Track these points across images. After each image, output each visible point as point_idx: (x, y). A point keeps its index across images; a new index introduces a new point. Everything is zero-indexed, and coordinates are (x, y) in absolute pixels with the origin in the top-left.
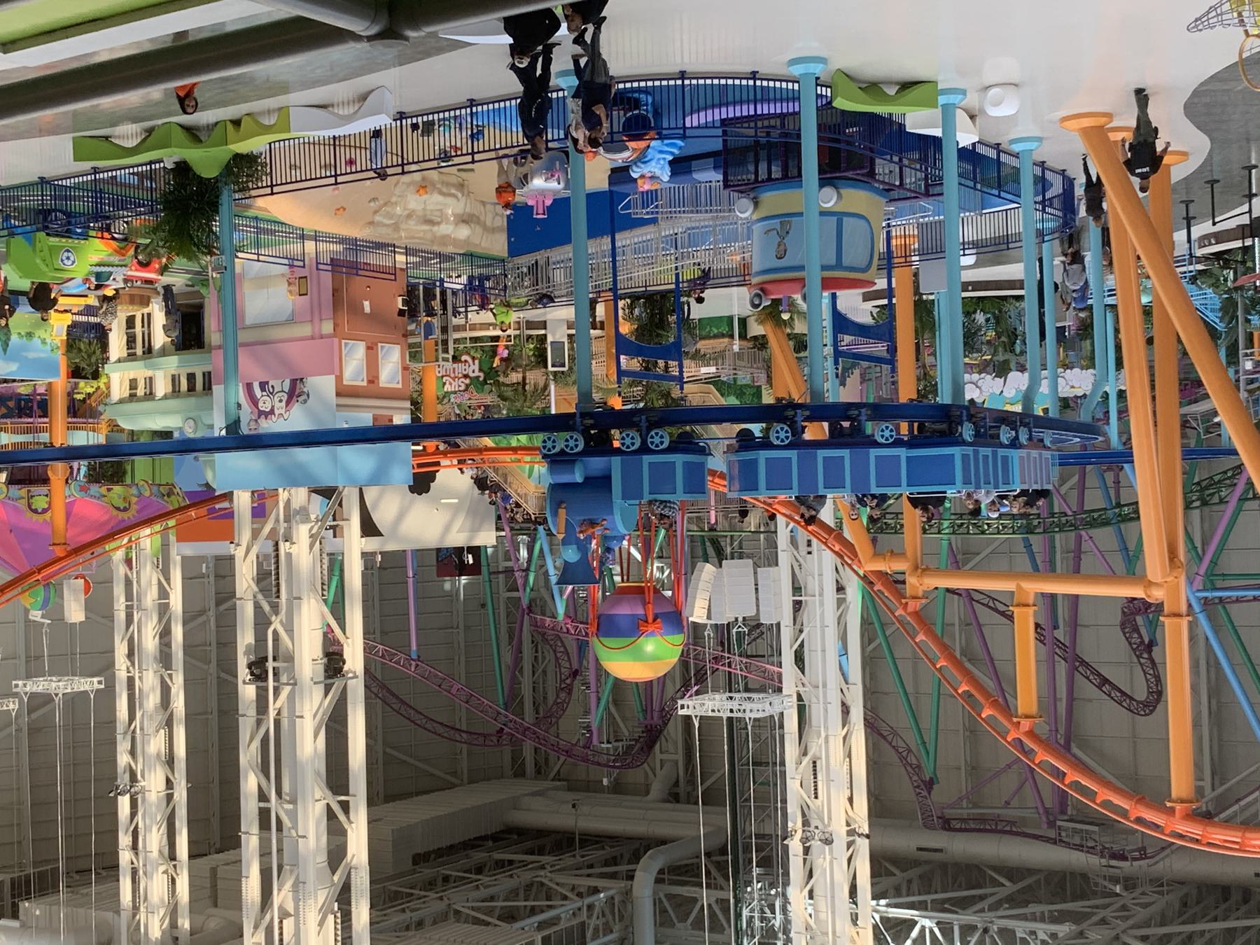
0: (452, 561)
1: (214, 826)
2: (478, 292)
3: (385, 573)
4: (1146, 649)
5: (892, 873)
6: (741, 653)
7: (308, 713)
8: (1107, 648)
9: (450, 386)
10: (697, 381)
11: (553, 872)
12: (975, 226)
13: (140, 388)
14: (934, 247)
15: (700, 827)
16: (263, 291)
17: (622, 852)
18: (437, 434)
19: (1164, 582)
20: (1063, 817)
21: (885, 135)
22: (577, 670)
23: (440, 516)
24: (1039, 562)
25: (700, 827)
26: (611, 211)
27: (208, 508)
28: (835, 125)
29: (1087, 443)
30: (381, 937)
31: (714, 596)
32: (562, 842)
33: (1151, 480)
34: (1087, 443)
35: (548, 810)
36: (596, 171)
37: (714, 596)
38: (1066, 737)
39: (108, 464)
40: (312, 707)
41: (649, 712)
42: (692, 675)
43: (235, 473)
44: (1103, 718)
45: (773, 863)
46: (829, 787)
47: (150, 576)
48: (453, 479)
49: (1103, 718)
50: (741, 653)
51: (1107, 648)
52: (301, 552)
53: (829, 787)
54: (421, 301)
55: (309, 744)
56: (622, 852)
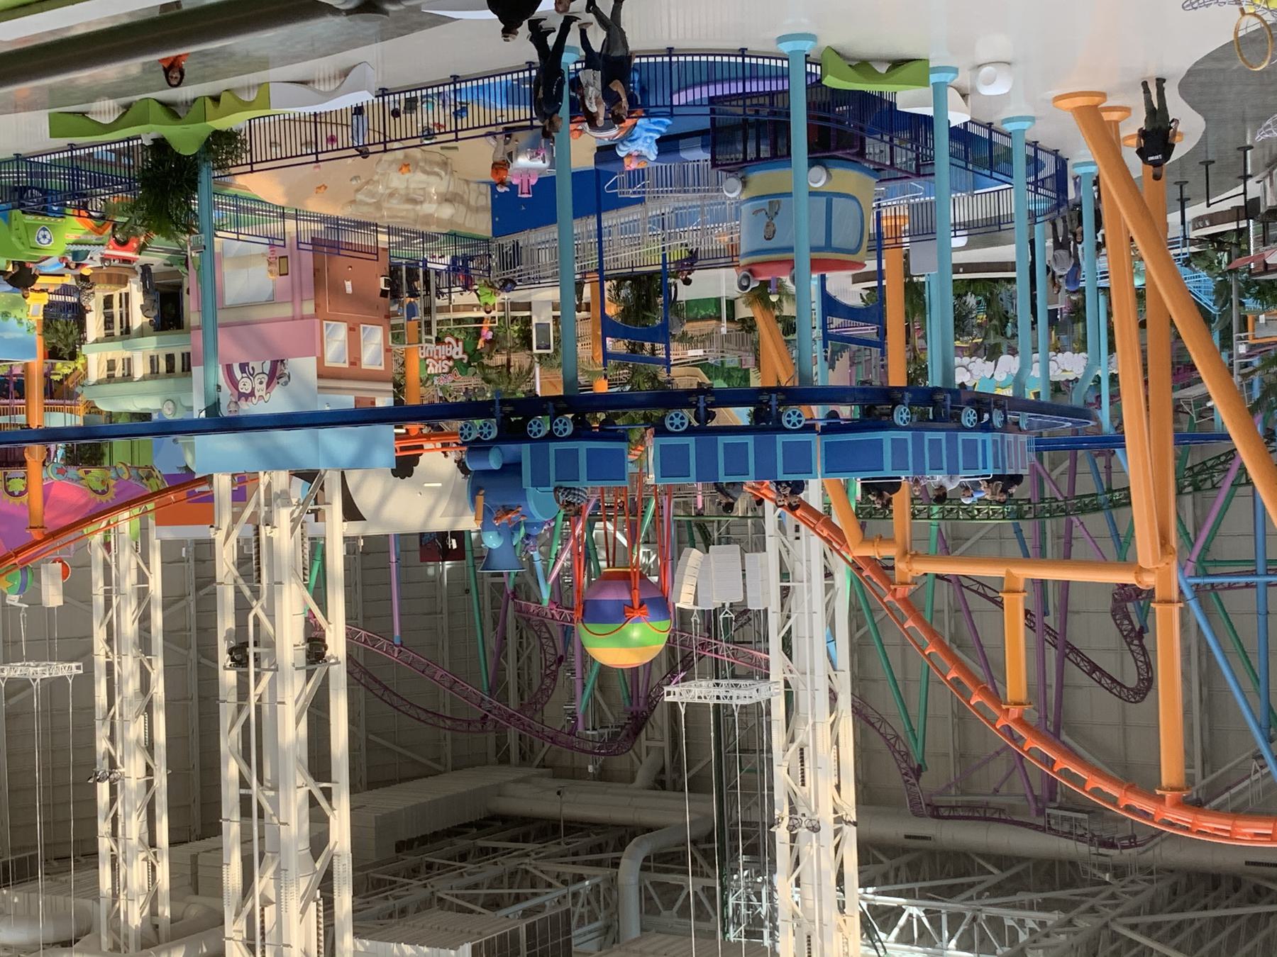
0: (435, 545)
1: (194, 813)
2: (462, 272)
3: (367, 557)
4: (1137, 637)
5: (879, 861)
6: (728, 639)
9: (434, 369)
11: (537, 859)
12: (966, 207)
13: (117, 369)
14: (924, 228)
15: (686, 814)
16: (243, 271)
17: (608, 839)
19: (1155, 568)
21: (877, 115)
22: (563, 656)
25: (686, 814)
26: (597, 191)
27: (188, 491)
28: (824, 103)
31: (701, 581)
32: (546, 830)
33: (1143, 465)
35: (532, 796)
37: (701, 581)
38: (1055, 724)
39: (86, 446)
40: (293, 693)
41: (635, 699)
42: (678, 661)
43: (215, 456)
45: (759, 851)
46: (816, 774)
47: (129, 559)
50: (728, 639)
51: (1097, 635)
52: (282, 536)
53: (816, 774)
54: (404, 281)
55: (291, 730)
56: (608, 839)
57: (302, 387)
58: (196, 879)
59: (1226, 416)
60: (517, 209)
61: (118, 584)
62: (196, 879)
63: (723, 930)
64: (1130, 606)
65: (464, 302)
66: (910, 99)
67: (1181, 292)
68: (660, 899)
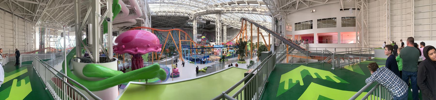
0: (212, 42)
1: (222, 30)
2: (210, 54)
3: (215, 41)
4: (181, 38)
5: (192, 28)
6: (199, 37)
7: (218, 35)
8: (183, 38)
9: (212, 50)
10: (201, 50)
11: (208, 28)
12: (188, 56)
13: (225, 49)
14: (190, 56)
15: (201, 30)
16: (220, 54)
17: (204, 28)
18: (213, 48)
19: (180, 41)
20: (185, 30)
21: (192, 61)
22: (206, 37)
23: (212, 44)
24: (211, 15)
25: (201, 30)
26: (205, 57)
27: (223, 44)
28: (194, 61)
29: (184, 46)
30: (139, 66)
31: (200, 40)
32: (207, 29)
33: (181, 45)
34: (184, 46)
35: (208, 30)
36: (205, 59)
37: (200, 40)
38: (185, 34)
39: (227, 46)
40: (218, 35)
41: (203, 35)
42: (201, 36)
43: (222, 46)
44: (183, 35)
45: (197, 28)
46: (195, 31)
47: (225, 41)
48: (212, 45)
49: (183, 35)
50: (199, 37)
51: (183, 38)
52: (219, 42)
53: (195, 31)
54: (213, 53)
55: (218, 34)
56: (204, 28)
57: (217, 49)
58: (222, 28)
59: (177, 47)
60: (208, 57)
61: (180, 7)
62: (222, 28)
63: (134, 65)
64: (181, 39)
65: (210, 52)
66: (190, 61)
67: (179, 52)
68: (202, 26)
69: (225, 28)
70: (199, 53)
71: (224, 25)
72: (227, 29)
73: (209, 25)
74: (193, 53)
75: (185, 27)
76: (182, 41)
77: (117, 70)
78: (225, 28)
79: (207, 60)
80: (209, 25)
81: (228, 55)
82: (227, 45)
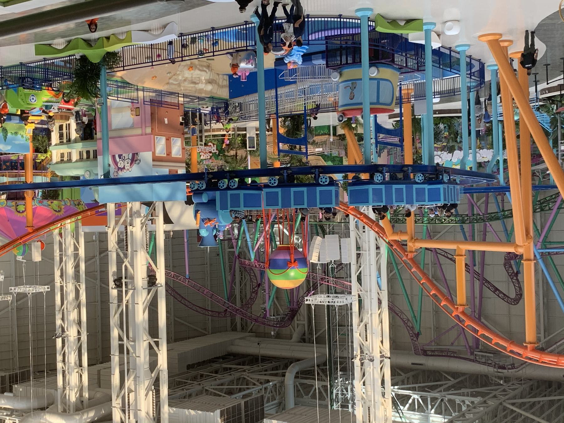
1: (99, 352)
2: (215, 115)
3: (174, 239)
4: (515, 276)
5: (400, 374)
6: (334, 276)
7: (141, 301)
9: (204, 158)
11: (249, 373)
12: (440, 85)
13: (65, 157)
14: (421, 95)
15: (314, 353)
17: (280, 364)
19: (523, 245)
21: (400, 44)
25: (314, 353)
26: (275, 78)
27: (96, 211)
28: (376, 39)
31: (321, 251)
33: (518, 199)
34: (487, 183)
35: (247, 346)
37: (321, 251)
38: (479, 314)
39: (52, 191)
40: (72, 333)
41: (292, 303)
42: (311, 286)
43: (108, 195)
44: (496, 306)
45: (347, 370)
46: (372, 336)
47: (70, 241)
49: (496, 306)
50: (334, 276)
51: (497, 275)
52: (137, 231)
53: (372, 336)
54: (190, 118)
55: (141, 316)
56: (280, 364)
58: (99, 381)
60: (240, 86)
62: (99, 381)
65: (217, 127)
68: (303, 391)
69: (73, 378)
70: (328, 119)
71: (81, 407)
72: (47, 369)
73: (237, 400)
74: (386, 121)
75: (476, 382)
76: (509, 237)
77: (492, 150)
78: (73, 378)
79: (251, 54)
80: (237, 400)
81: (45, 96)
82: (49, 208)
